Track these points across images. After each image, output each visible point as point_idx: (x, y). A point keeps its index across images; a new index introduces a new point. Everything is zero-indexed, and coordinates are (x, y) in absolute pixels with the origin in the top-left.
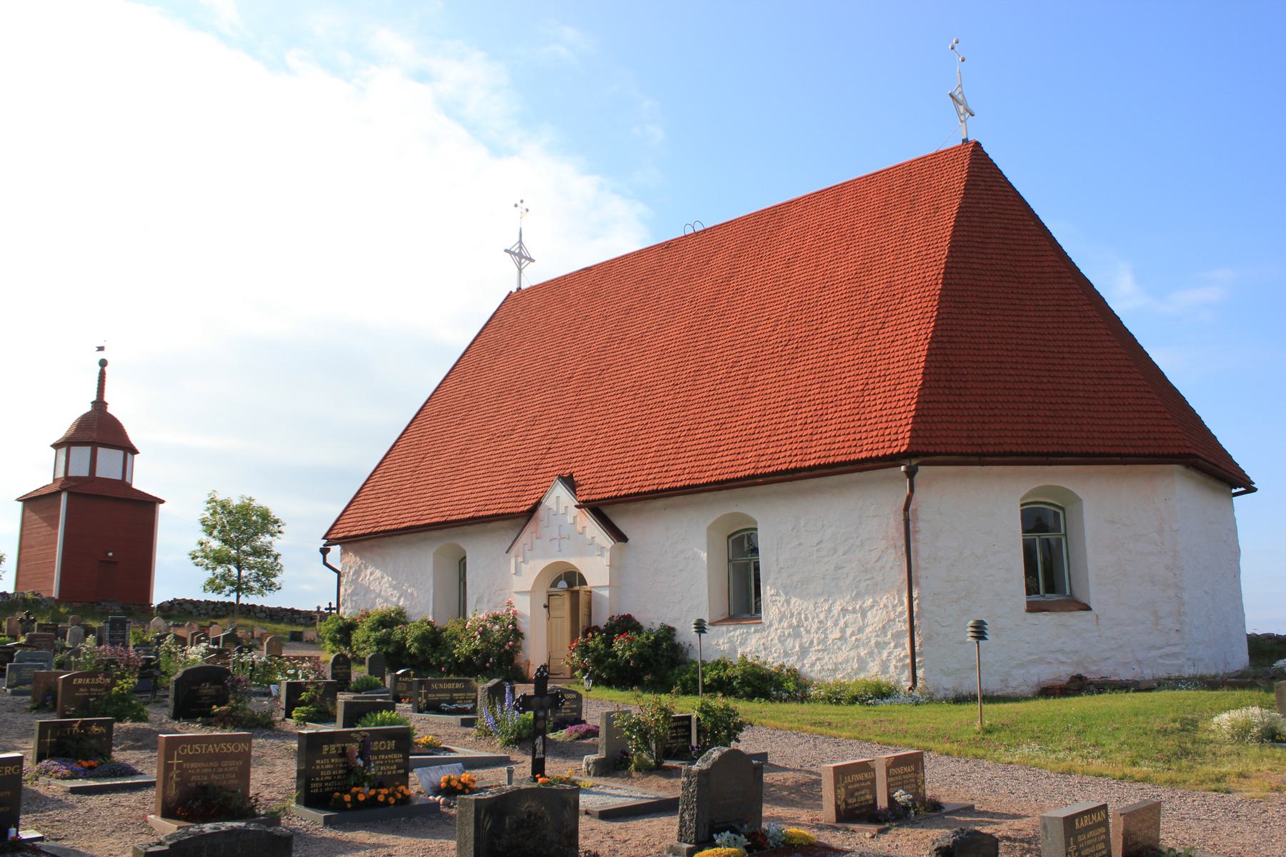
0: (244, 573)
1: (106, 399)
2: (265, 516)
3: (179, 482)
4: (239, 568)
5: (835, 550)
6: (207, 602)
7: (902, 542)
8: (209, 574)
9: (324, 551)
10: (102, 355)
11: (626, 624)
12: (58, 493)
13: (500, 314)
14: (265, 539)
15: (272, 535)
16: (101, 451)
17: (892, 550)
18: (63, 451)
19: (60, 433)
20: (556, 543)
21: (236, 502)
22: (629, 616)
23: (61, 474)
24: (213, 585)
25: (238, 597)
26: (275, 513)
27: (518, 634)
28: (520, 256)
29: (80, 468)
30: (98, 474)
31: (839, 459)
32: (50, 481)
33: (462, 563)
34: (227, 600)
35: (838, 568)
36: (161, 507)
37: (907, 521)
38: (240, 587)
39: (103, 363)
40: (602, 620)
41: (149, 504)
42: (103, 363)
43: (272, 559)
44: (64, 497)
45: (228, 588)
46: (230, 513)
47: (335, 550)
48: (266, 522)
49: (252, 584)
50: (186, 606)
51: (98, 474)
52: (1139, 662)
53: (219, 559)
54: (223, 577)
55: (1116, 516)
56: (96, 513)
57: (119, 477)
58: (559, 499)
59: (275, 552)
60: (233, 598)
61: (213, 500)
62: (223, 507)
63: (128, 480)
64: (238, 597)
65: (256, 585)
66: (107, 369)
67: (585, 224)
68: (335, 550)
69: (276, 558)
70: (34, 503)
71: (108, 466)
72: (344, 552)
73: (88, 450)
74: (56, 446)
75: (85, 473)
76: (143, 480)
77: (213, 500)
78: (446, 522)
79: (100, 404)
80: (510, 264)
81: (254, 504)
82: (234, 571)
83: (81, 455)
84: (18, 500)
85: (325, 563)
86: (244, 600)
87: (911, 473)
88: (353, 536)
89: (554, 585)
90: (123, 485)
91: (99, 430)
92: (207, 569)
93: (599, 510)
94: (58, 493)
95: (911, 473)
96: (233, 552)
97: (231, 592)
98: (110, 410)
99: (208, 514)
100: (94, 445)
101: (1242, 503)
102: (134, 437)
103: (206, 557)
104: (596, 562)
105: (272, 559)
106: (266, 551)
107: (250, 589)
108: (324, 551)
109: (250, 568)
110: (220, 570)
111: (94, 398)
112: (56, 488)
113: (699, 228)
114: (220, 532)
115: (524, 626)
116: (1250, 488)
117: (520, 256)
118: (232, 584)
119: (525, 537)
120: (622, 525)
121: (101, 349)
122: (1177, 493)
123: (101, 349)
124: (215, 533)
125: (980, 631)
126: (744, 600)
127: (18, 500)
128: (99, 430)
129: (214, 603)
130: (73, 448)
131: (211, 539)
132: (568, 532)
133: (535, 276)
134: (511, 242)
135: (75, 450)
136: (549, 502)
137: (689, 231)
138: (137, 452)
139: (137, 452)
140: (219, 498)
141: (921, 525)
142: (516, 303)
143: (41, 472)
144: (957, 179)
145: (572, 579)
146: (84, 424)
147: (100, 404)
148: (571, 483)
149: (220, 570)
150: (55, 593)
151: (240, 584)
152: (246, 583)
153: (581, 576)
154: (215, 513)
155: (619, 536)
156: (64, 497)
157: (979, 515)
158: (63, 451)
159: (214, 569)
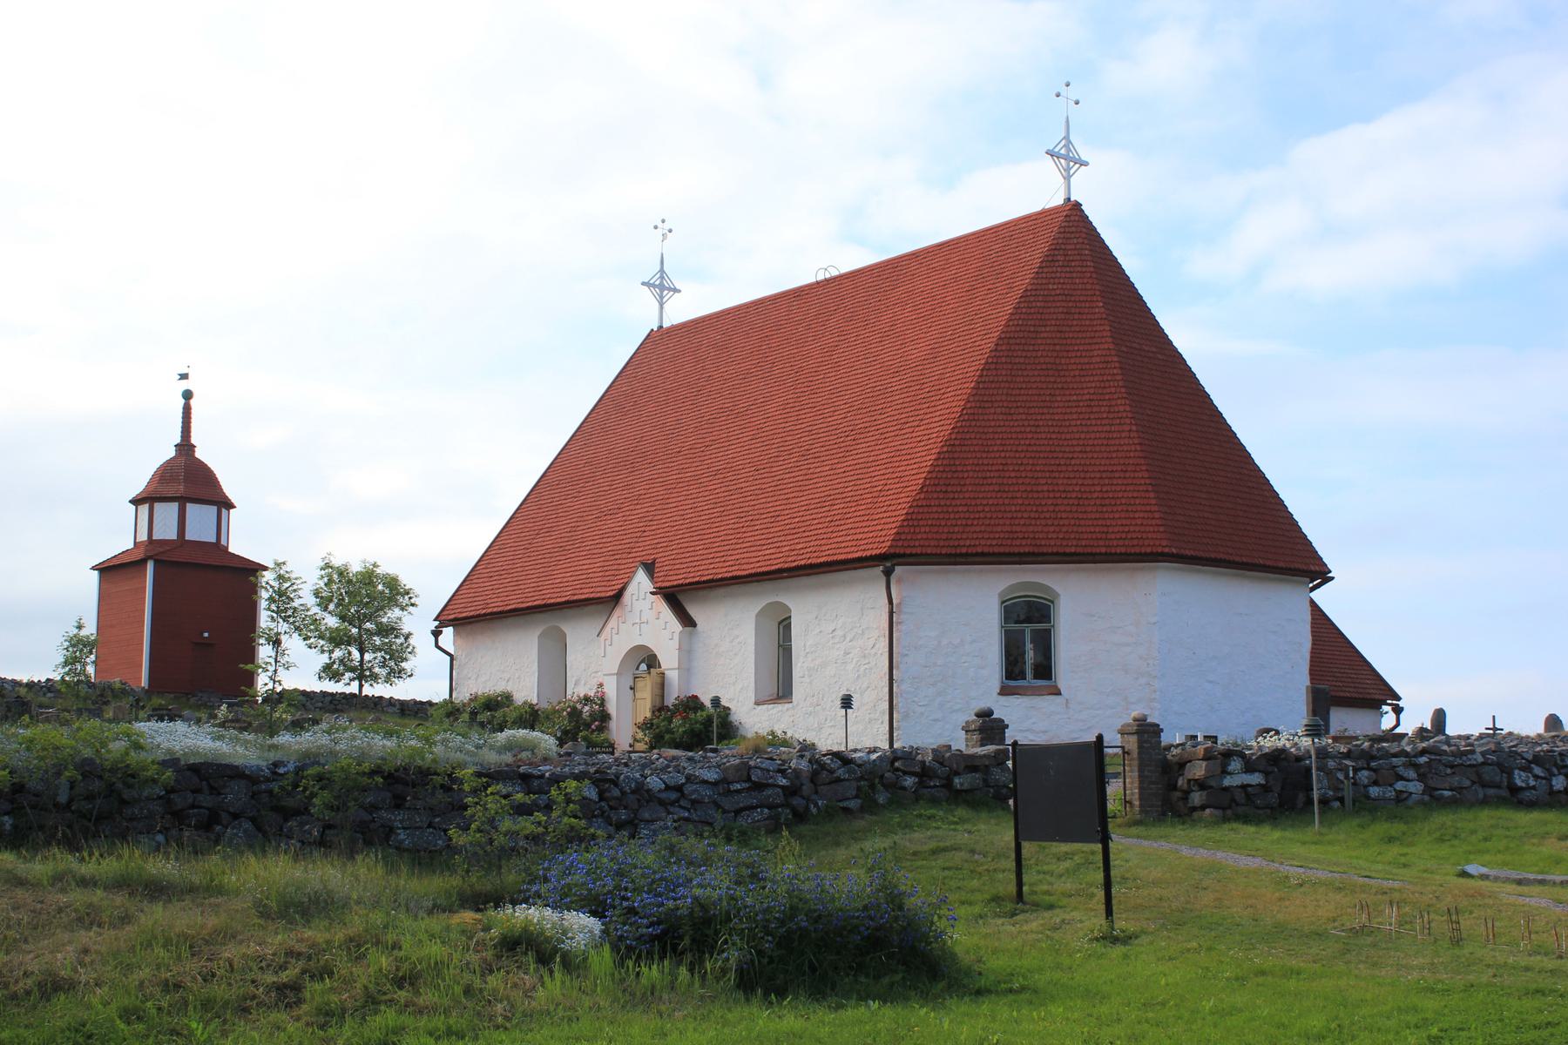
0: (367, 657)
1: (193, 441)
2: (392, 583)
3: (281, 529)
4: (362, 652)
6: (324, 694)
8: (325, 659)
9: (436, 633)
10: (185, 385)
11: (692, 703)
14: (394, 614)
15: (403, 609)
16: (190, 507)
18: (144, 509)
19: (139, 486)
21: (356, 568)
23: (143, 537)
24: (329, 672)
25: (361, 686)
26: (406, 580)
27: (604, 717)
28: (662, 287)
29: (166, 529)
32: (131, 546)
34: (348, 690)
38: (362, 674)
39: (188, 395)
40: (670, 701)
42: (188, 395)
43: (402, 640)
44: (150, 566)
45: (348, 675)
46: (350, 582)
47: (448, 632)
48: (395, 593)
49: (377, 670)
50: (23, 691)
53: (337, 639)
54: (341, 661)
56: (188, 591)
58: (641, 583)
59: (406, 630)
60: (354, 688)
61: (327, 566)
62: (341, 574)
63: (223, 542)
64: (361, 686)
65: (383, 672)
66: (192, 402)
68: (448, 632)
69: (407, 637)
70: (109, 571)
72: (456, 633)
73: (175, 506)
74: (136, 502)
75: (172, 535)
76: (241, 544)
77: (327, 566)
78: (545, 606)
79: (185, 447)
80: (648, 298)
81: (378, 571)
82: (356, 654)
83: (167, 514)
84: (93, 568)
85: (437, 646)
86: (368, 690)
87: (888, 573)
88: (468, 615)
90: (219, 548)
91: (187, 481)
92: (323, 652)
93: (674, 597)
94: (143, 562)
95: (888, 573)
96: (355, 631)
97: (352, 680)
98: (199, 454)
99: (322, 584)
100: (183, 501)
103: (321, 637)
105: (402, 640)
106: (394, 629)
107: (375, 678)
108: (436, 633)
109: (376, 649)
110: (338, 654)
111: (178, 440)
112: (139, 555)
113: (835, 273)
114: (337, 606)
115: (612, 708)
118: (352, 670)
119: (613, 622)
120: (693, 611)
121: (184, 377)
123: (184, 377)
124: (331, 607)
125: (847, 702)
127: (93, 568)
128: (187, 481)
129: (332, 694)
130: (157, 506)
131: (326, 614)
132: (644, 617)
133: (681, 310)
134: (650, 272)
135: (159, 507)
137: (821, 277)
138: (233, 507)
139: (233, 507)
140: (337, 562)
142: (660, 343)
143: (119, 535)
145: (652, 661)
146: (165, 474)
147: (185, 447)
148: (650, 568)
149: (338, 654)
150: (144, 683)
151: (363, 670)
152: (370, 669)
154: (330, 582)
155: (687, 621)
156: (150, 566)
158: (144, 509)
159: (331, 652)
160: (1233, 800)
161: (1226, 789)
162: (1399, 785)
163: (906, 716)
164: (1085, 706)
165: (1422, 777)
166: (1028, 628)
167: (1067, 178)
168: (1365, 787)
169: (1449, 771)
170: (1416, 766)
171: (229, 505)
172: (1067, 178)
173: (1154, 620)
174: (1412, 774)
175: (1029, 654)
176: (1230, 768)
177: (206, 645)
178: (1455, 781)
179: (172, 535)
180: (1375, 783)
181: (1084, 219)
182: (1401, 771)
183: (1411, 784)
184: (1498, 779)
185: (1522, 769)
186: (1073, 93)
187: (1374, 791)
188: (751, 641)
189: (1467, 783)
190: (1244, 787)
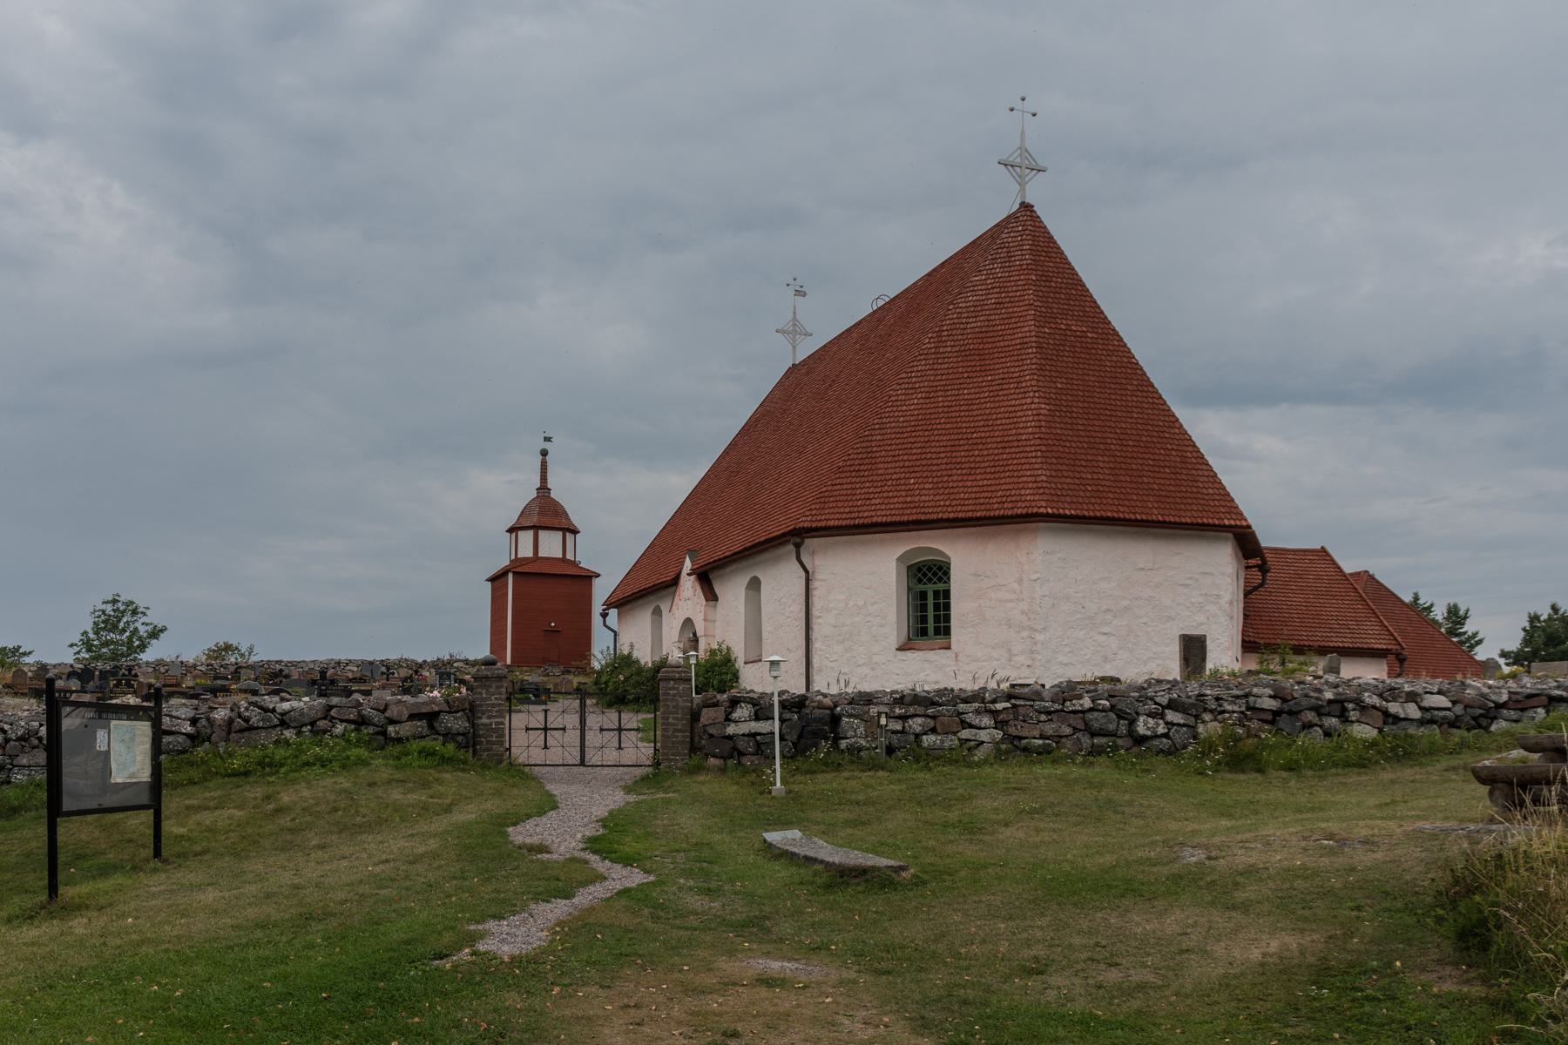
10: (547, 445)
19: (512, 520)
22: (1323, 553)
29: (526, 551)
31: (831, 523)
36: (596, 582)
42: (544, 453)
44: (510, 576)
57: (803, 691)
68: (613, 613)
71: (551, 545)
73: (531, 533)
74: (510, 530)
75: (530, 554)
83: (526, 538)
91: (546, 514)
95: (798, 546)
100: (536, 528)
102: (576, 519)
117: (794, 331)
121: (547, 439)
123: (547, 439)
128: (546, 514)
135: (521, 533)
147: (544, 488)
156: (510, 576)
160: (735, 748)
161: (730, 738)
162: (965, 734)
163: (820, 670)
164: (974, 660)
165: (1000, 724)
166: (930, 589)
167: (1022, 185)
168: (917, 736)
169: (1043, 717)
170: (994, 713)
171: (575, 532)
172: (1022, 185)
173: (1035, 576)
174: (986, 720)
175: (929, 611)
176: (735, 715)
177: (555, 631)
178: (1049, 729)
179: (530, 554)
180: (934, 730)
181: (1035, 218)
182: (970, 718)
183: (982, 732)
184: (1111, 727)
185: (1151, 715)
186: (1029, 106)
187: (929, 740)
188: (742, 610)
189: (1067, 730)
190: (753, 735)
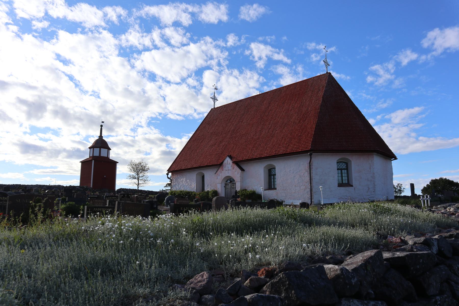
5: (294, 172)
7: (309, 171)
9: (168, 174)
10: (102, 124)
12: (92, 160)
13: (208, 116)
16: (102, 149)
17: (306, 173)
18: (92, 149)
20: (227, 172)
23: (91, 155)
29: (97, 154)
30: (101, 155)
33: (203, 177)
35: (294, 177)
37: (310, 166)
41: (114, 164)
44: (93, 161)
47: (170, 174)
51: (101, 155)
52: (364, 199)
55: (360, 165)
58: (228, 161)
67: (236, 88)
71: (104, 152)
73: (99, 149)
75: (98, 155)
79: (101, 137)
83: (97, 150)
88: (176, 169)
89: (227, 181)
91: (101, 144)
94: (92, 160)
100: (100, 148)
101: (394, 162)
104: (235, 173)
108: (168, 174)
116: (396, 158)
120: (244, 167)
122: (377, 161)
123: (103, 122)
126: (271, 186)
128: (101, 144)
132: (229, 168)
136: (225, 162)
141: (313, 167)
142: (214, 111)
144: (324, 83)
146: (97, 142)
147: (101, 137)
148: (231, 157)
153: (233, 179)
155: (242, 170)
156: (93, 161)
157: (327, 165)
